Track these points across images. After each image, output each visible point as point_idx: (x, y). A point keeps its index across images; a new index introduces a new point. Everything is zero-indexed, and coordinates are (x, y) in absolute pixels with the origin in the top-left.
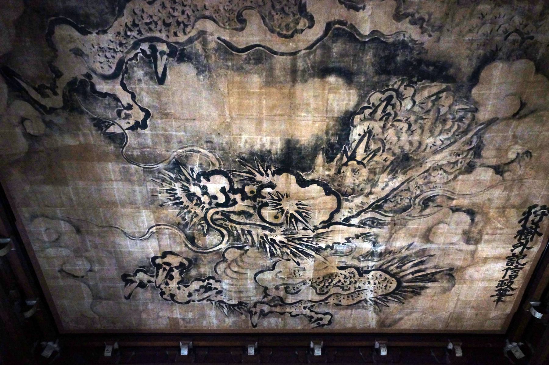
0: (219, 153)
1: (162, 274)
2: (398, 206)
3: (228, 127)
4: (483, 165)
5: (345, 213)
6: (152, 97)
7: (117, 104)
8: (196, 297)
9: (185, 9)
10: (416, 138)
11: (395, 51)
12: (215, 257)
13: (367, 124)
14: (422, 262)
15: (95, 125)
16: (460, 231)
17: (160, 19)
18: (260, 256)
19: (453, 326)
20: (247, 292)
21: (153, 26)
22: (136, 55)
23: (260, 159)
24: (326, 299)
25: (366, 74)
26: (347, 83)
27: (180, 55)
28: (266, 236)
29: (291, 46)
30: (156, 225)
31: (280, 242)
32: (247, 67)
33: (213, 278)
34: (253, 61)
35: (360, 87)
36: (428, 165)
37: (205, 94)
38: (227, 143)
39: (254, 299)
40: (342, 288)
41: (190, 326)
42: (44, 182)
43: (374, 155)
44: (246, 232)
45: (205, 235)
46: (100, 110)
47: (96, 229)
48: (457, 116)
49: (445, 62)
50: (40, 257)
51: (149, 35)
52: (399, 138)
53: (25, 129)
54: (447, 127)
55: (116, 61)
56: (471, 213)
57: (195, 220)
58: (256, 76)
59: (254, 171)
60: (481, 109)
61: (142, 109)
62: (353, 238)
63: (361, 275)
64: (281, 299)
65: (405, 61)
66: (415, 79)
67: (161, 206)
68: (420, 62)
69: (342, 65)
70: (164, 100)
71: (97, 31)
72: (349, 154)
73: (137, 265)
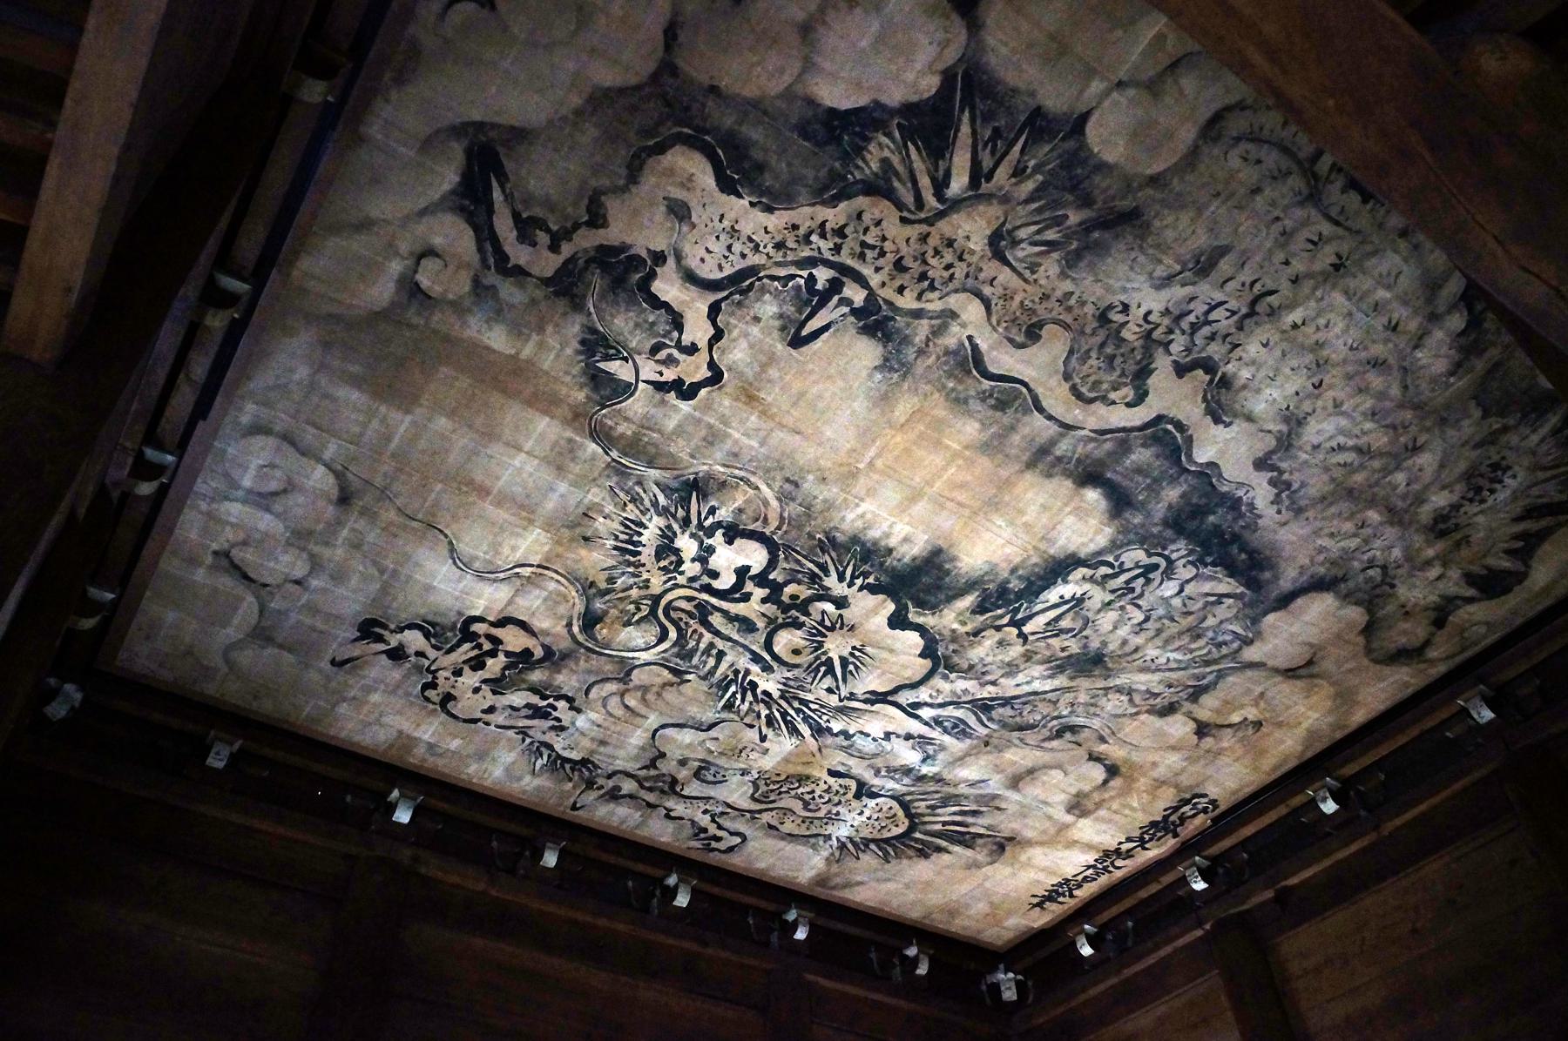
0: (793, 509)
1: (466, 651)
2: (1018, 719)
3: (853, 475)
4: (1189, 715)
5: (923, 694)
6: (754, 356)
7: (670, 332)
8: (499, 718)
9: (957, 263)
10: (1138, 640)
11: (1216, 505)
12: (609, 667)
13: (1087, 586)
14: (975, 813)
15: (583, 342)
16: (1073, 791)
17: (898, 251)
18: (703, 698)
19: (940, 923)
20: (616, 747)
21: (870, 254)
22: (793, 277)
23: (864, 557)
24: (760, 812)
25: (1148, 515)
26: (1110, 512)
27: (874, 321)
28: (747, 672)
29: (1076, 414)
30: (539, 566)
31: (765, 693)
32: (975, 405)
33: (570, 700)
34: (993, 402)
35: (1124, 530)
36: (1118, 682)
37: (860, 405)
38: (825, 501)
39: (620, 764)
40: (806, 805)
41: (441, 763)
42: (356, 382)
43: (1056, 635)
44: (714, 652)
45: (628, 624)
46: (622, 323)
47: (392, 515)
48: (1220, 639)
49: (1268, 559)
50: (195, 507)
51: (850, 262)
52: (1111, 627)
53: (416, 272)
54: (1193, 646)
55: (740, 265)
56: (1113, 771)
57: (634, 593)
58: (977, 425)
59: (832, 568)
60: (1257, 644)
61: (712, 365)
62: (898, 736)
63: (858, 796)
64: (674, 781)
65: (1216, 527)
66: (1209, 560)
67: (586, 539)
68: (1236, 538)
69: (1125, 483)
70: (773, 373)
71: (755, 200)
72: (1020, 616)
73: (418, 616)
